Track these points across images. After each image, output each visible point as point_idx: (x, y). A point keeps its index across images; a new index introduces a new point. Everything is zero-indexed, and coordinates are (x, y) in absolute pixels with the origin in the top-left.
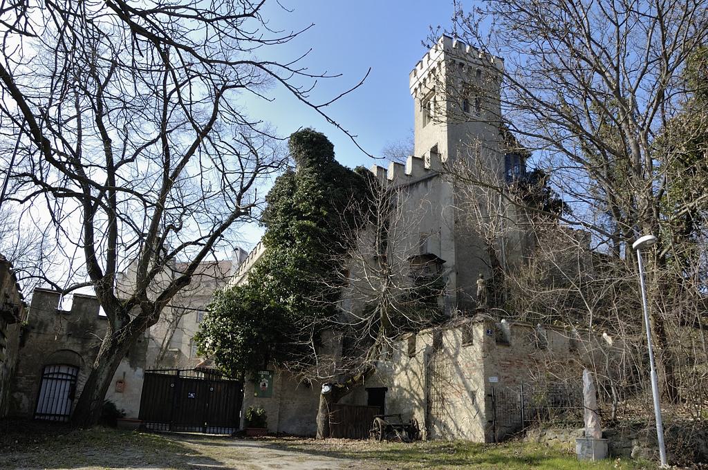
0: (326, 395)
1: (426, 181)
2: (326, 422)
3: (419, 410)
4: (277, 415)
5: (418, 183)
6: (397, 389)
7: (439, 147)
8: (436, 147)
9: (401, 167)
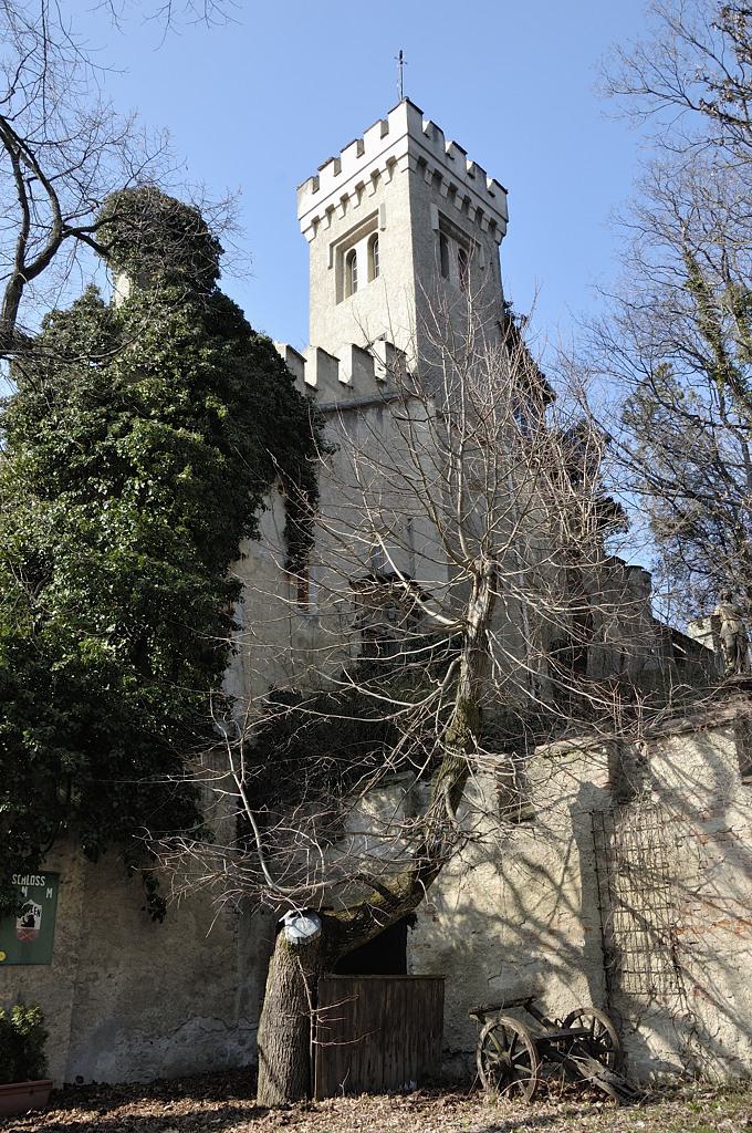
0: (298, 948)
1: (379, 405)
2: (299, 1043)
3: (567, 979)
4: (67, 1026)
5: (365, 406)
6: (458, 919)
9: (332, 360)
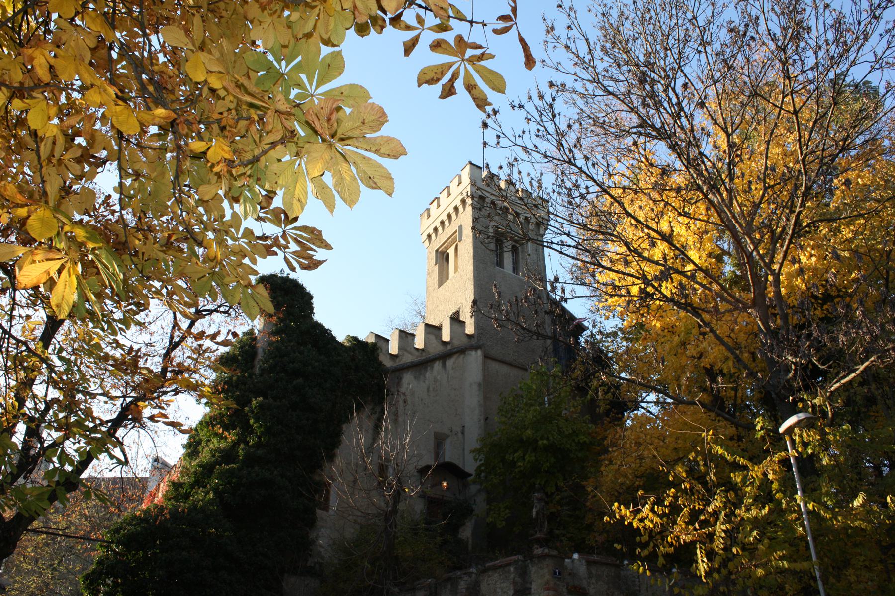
1: (443, 357)
7: (461, 314)
8: (457, 313)
